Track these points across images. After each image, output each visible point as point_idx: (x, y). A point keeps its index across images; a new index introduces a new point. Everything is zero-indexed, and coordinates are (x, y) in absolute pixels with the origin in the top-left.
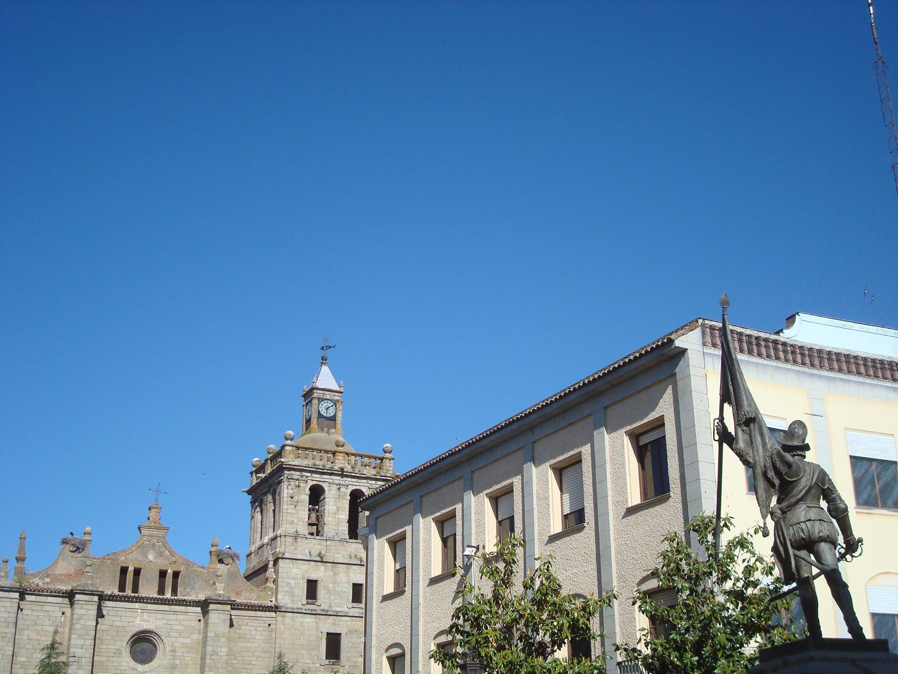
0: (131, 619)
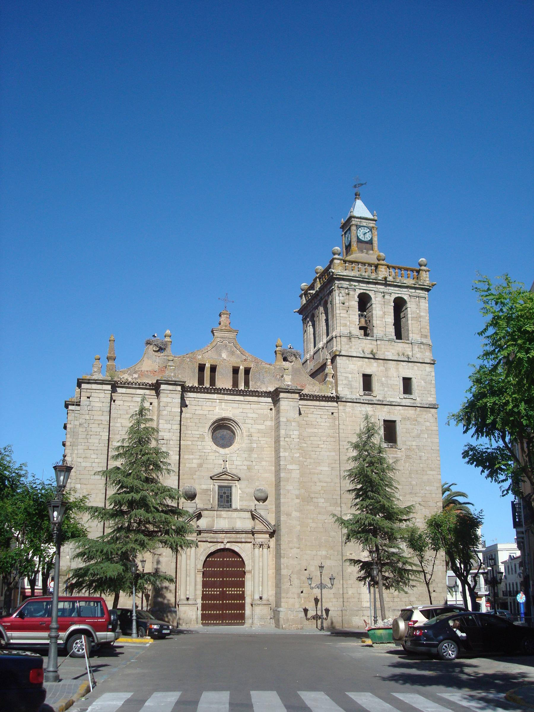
0: (211, 408)
